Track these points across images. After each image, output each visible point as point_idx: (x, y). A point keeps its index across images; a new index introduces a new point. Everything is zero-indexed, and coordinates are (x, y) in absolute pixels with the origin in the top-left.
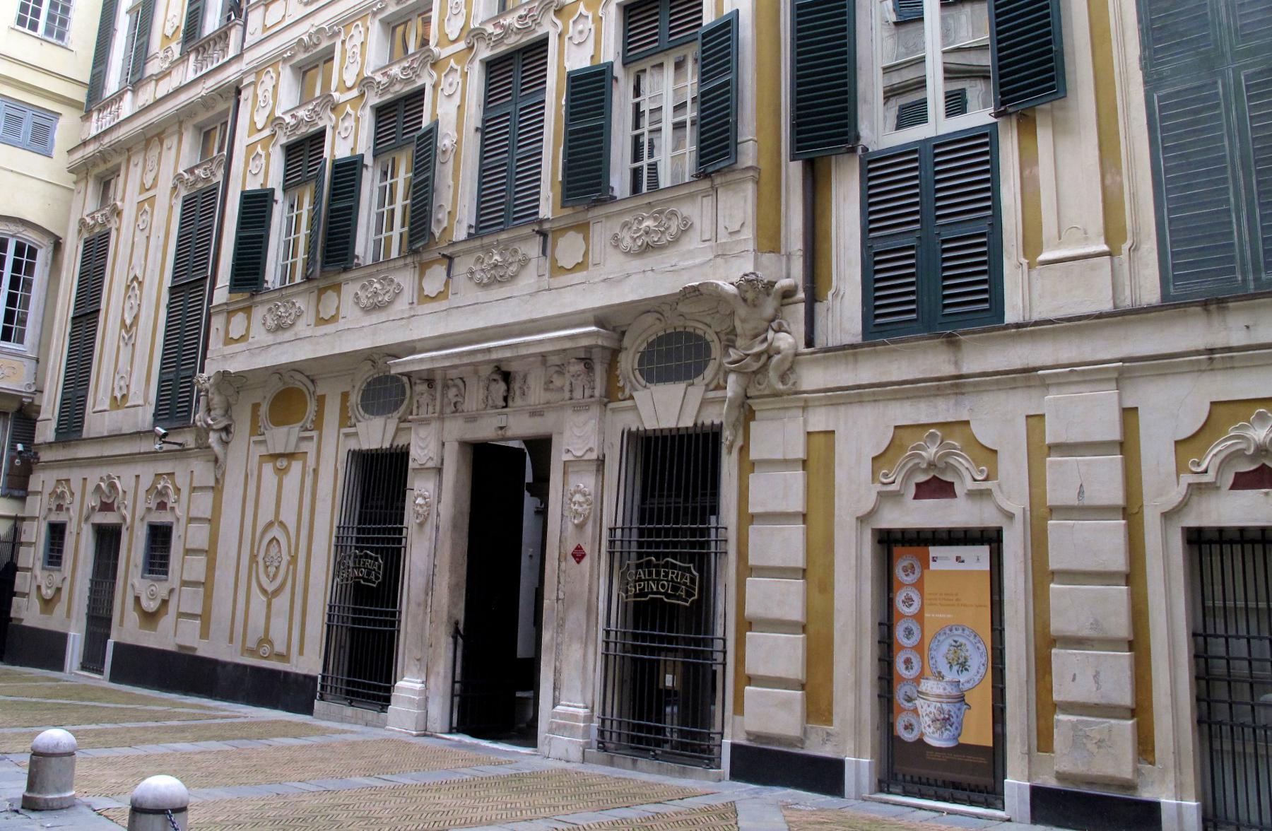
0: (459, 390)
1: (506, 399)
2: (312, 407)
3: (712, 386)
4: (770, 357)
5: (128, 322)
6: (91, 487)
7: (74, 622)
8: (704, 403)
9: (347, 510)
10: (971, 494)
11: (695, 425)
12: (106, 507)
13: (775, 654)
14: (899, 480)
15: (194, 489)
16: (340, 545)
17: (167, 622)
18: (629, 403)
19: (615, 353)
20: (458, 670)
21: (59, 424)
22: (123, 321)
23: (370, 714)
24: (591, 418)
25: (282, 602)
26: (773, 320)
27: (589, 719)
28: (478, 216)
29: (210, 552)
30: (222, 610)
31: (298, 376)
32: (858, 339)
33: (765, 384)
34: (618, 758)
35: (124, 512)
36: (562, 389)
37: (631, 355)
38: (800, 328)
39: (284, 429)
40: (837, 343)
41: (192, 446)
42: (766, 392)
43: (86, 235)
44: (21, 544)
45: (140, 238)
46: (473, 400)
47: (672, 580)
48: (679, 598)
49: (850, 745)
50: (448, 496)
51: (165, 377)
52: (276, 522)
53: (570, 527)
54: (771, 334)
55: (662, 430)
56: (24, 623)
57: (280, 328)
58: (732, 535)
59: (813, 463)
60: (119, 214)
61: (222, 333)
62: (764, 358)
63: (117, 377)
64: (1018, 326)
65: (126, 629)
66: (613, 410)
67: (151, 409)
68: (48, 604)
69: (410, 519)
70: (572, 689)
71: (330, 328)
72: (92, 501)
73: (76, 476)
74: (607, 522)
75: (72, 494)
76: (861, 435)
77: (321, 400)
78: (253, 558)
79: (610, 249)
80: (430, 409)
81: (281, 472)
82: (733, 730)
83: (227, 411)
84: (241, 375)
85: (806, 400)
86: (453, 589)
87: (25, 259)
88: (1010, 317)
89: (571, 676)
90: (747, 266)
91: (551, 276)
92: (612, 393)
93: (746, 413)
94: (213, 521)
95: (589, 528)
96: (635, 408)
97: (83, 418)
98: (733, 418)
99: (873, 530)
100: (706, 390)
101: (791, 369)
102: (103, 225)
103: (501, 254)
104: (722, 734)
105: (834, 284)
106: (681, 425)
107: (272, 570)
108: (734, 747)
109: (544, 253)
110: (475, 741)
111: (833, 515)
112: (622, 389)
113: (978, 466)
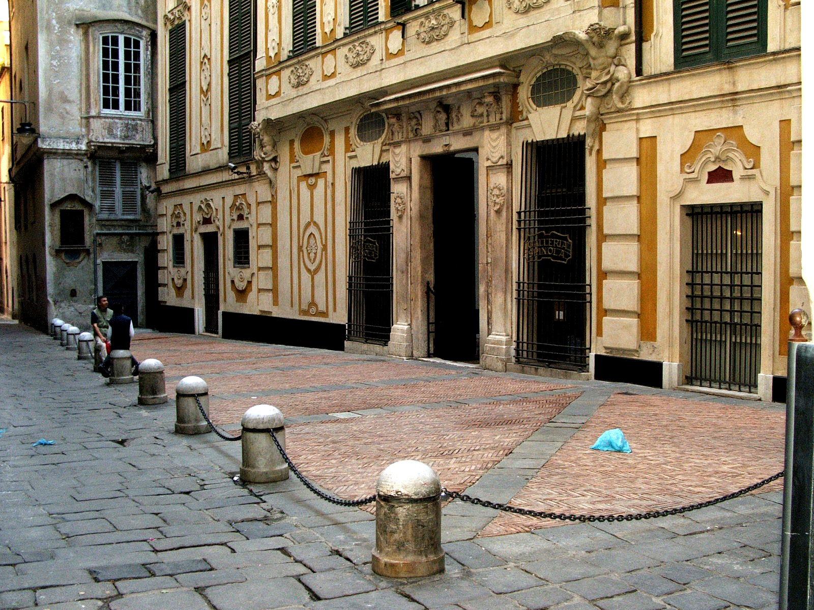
0: (418, 120)
1: (447, 125)
2: (327, 139)
3: (578, 108)
4: (613, 84)
5: (205, 88)
6: (195, 208)
7: (197, 300)
8: (574, 119)
9: (355, 211)
10: (743, 178)
11: (568, 136)
12: (207, 221)
13: (619, 294)
14: (697, 171)
15: (259, 204)
16: (352, 235)
17: (252, 296)
18: (525, 123)
19: (515, 86)
20: (432, 314)
21: (170, 166)
22: (201, 88)
23: (378, 348)
24: (501, 135)
25: (320, 277)
26: (615, 57)
27: (508, 343)
28: (351, 20)
29: (274, 247)
30: (284, 285)
31: (315, 118)
32: (672, 68)
33: (611, 103)
34: (527, 368)
35: (218, 223)
36: (482, 115)
37: (526, 88)
38: (632, 62)
39: (311, 156)
40: (658, 72)
41: (255, 174)
42: (612, 110)
43: (170, 27)
44: (159, 251)
45: (205, 25)
46: (427, 128)
47: (556, 247)
48: (561, 258)
49: (666, 354)
50: (416, 194)
51: (233, 126)
52: (312, 222)
53: (492, 214)
54: (612, 68)
55: (547, 141)
56: (167, 304)
57: (299, 85)
58: (593, 213)
59: (643, 159)
60: (189, 9)
61: (264, 92)
62: (609, 85)
63: (203, 129)
64: (774, 54)
65: (228, 304)
66: (517, 128)
67: (226, 150)
68: (180, 290)
69: (394, 215)
70: (500, 324)
71: (332, 82)
72: (198, 217)
73: (185, 201)
74: (516, 208)
75: (185, 214)
76: (673, 138)
77: (332, 134)
78: (300, 249)
79: (506, 10)
80: (400, 135)
81: (312, 187)
82: (597, 347)
83: (274, 145)
84: (279, 121)
85: (638, 114)
86: (424, 261)
87: (132, 49)
88: (772, 47)
89: (497, 316)
90: (592, 17)
91: (469, 34)
92: (515, 118)
93: (599, 124)
94: (273, 225)
95: (504, 213)
96: (529, 126)
97: (185, 160)
98: (591, 131)
99: (683, 206)
100: (574, 111)
101: (627, 91)
102: (180, 18)
103: (436, 19)
104: (590, 349)
105: (655, 28)
106: (559, 136)
107: (312, 255)
108: (597, 356)
109: (463, 16)
110: (443, 361)
111: (656, 196)
112: (521, 112)
113: (748, 158)
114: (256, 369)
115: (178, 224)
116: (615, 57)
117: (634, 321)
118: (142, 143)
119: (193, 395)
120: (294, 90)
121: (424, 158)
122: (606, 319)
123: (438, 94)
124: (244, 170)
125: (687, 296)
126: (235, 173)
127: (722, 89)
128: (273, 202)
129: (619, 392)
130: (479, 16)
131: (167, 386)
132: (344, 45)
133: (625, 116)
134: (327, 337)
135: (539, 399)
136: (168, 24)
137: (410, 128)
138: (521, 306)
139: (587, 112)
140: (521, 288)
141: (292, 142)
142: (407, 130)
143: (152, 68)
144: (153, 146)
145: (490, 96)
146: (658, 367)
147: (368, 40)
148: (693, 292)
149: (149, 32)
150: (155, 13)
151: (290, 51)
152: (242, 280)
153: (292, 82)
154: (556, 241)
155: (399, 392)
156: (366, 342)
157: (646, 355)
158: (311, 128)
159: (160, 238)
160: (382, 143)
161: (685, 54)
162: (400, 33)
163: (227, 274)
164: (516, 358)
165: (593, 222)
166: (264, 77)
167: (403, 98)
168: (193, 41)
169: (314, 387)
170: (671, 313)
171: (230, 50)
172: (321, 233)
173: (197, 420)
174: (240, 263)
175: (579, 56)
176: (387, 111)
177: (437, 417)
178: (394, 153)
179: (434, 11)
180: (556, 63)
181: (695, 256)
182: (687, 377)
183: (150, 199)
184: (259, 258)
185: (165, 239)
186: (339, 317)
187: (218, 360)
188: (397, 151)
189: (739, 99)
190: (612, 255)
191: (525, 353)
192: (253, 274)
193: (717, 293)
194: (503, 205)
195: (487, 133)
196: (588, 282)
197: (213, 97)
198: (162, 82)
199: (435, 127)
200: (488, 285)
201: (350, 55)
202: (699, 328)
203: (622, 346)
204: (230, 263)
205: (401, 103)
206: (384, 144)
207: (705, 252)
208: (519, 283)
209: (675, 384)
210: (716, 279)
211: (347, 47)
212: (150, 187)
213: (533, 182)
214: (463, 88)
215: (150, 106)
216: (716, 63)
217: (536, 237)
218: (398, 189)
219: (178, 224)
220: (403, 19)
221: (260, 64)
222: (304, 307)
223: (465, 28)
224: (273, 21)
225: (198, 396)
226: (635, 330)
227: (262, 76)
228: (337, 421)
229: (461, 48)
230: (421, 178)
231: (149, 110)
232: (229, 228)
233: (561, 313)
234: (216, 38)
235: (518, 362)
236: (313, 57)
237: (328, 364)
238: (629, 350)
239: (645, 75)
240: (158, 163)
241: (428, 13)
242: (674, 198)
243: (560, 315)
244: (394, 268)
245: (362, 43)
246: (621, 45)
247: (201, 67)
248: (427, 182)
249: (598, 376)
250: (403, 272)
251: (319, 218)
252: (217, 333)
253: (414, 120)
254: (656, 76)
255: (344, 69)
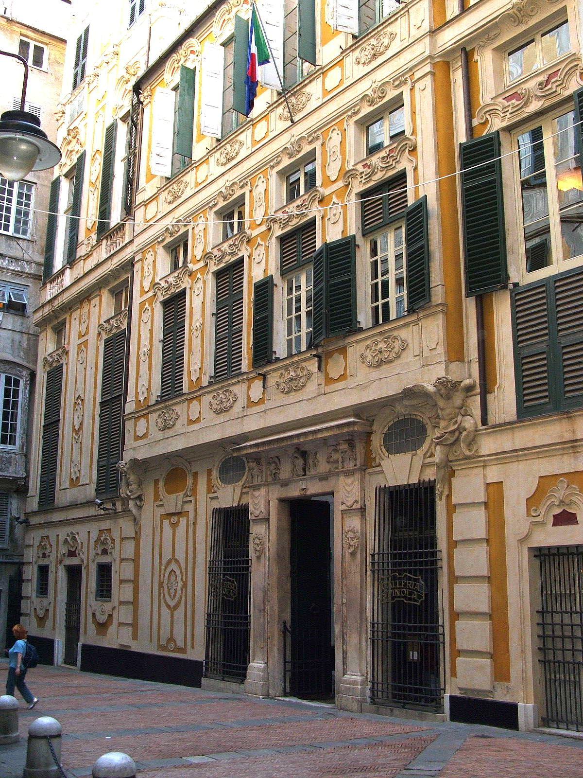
1: (304, 470)
2: (190, 481)
5: (77, 427)
6: (61, 541)
7: (57, 630)
8: (424, 466)
9: (215, 550)
11: (419, 481)
12: (72, 554)
13: (472, 634)
14: (542, 514)
15: (123, 539)
17: (112, 629)
18: (378, 469)
19: (369, 434)
20: (288, 653)
21: (40, 499)
22: (74, 427)
23: (234, 686)
25: (179, 614)
27: (363, 683)
29: (135, 582)
32: (515, 418)
33: (459, 451)
34: (382, 709)
35: (82, 556)
36: (337, 461)
38: (477, 412)
39: (174, 495)
40: (502, 421)
42: (461, 458)
46: (285, 472)
47: (409, 589)
51: (101, 464)
52: (173, 559)
53: (347, 555)
54: (459, 418)
57: (165, 428)
58: (444, 555)
59: (491, 505)
60: (67, 353)
61: (132, 434)
62: (457, 434)
63: (73, 465)
65: (89, 636)
67: (94, 486)
68: (41, 621)
69: (252, 555)
70: (355, 666)
71: (196, 427)
72: (64, 550)
73: (52, 533)
74: (370, 551)
76: (519, 482)
77: (195, 476)
78: (161, 585)
79: (359, 364)
81: (174, 526)
82: (451, 689)
83: (140, 484)
84: (145, 461)
85: (485, 461)
86: (281, 601)
89: (352, 655)
90: (439, 371)
92: (369, 464)
93: (449, 471)
94: (136, 560)
95: (358, 556)
96: (382, 472)
101: (473, 440)
102: (58, 361)
103: (295, 371)
104: (444, 690)
105: (498, 381)
107: (172, 591)
108: (451, 697)
109: (320, 369)
110: (299, 701)
114: (111, 706)
115: (44, 555)
116: (462, 408)
117: (487, 662)
118: (15, 475)
119: (45, 737)
120: (161, 432)
121: (282, 501)
122: (459, 660)
123: (295, 441)
124: (109, 506)
125: (539, 636)
126: (101, 509)
127: (563, 438)
128: (137, 539)
129: (475, 734)
130: (335, 368)
131: (20, 723)
132: (208, 393)
133: (473, 463)
134: (183, 673)
135: (394, 742)
136: (47, 366)
137: (269, 472)
138: (376, 659)
139: (436, 459)
140: (376, 637)
141: (156, 482)
142: (266, 473)
143: (29, 406)
144: (25, 478)
145: (345, 444)
146: (512, 709)
147: (231, 389)
148: (544, 632)
149: (29, 372)
150: (36, 355)
151: (158, 396)
152: (103, 613)
153: (158, 424)
154: (409, 583)
155: (253, 734)
156: (223, 680)
157: (501, 696)
158: (175, 469)
159: (25, 568)
160: (243, 486)
161: (526, 404)
162: (261, 383)
163: (88, 607)
164: (371, 698)
165: (444, 564)
166: (133, 420)
167: (263, 444)
168: (69, 382)
169: (169, 727)
170: (523, 652)
171: (103, 392)
172: (181, 572)
173: (48, 765)
174: (102, 596)
175: (428, 406)
176: (248, 456)
177: (292, 763)
178: (254, 496)
179: (293, 363)
180: (407, 412)
181: (545, 597)
182: (543, 719)
183: (19, 529)
184: (121, 592)
185: (31, 569)
186: (197, 653)
187: (75, 694)
188: (257, 493)
189: (579, 446)
190: (463, 597)
191: (380, 693)
192: (115, 607)
193: (568, 633)
194: (358, 547)
195: (342, 478)
196: (440, 623)
197: (85, 435)
198: (37, 418)
199: (293, 471)
200: (343, 626)
201: (214, 402)
202: (552, 668)
203: (477, 687)
204: (92, 597)
205: (261, 449)
206: (244, 487)
207: (554, 592)
208: (373, 624)
209: (532, 726)
210: (567, 619)
211: (212, 395)
212: (19, 518)
213: (386, 527)
214: (320, 436)
215: (24, 440)
216: (556, 413)
217: (390, 579)
218: (257, 530)
219: (44, 555)
220: (265, 370)
221: (130, 407)
222: (163, 642)
223: (322, 380)
224: (144, 367)
225: (50, 737)
226: (488, 670)
227: (130, 418)
228: (191, 765)
229: (318, 398)
230: (279, 520)
231: (23, 445)
232: (93, 561)
233: (415, 653)
234: (90, 381)
235: (373, 702)
236: (180, 402)
237: (184, 702)
238: (485, 691)
239: (490, 424)
240: (29, 495)
241: (288, 365)
242: (522, 541)
243: (414, 655)
244: (252, 609)
245: (226, 391)
246: (467, 397)
247: (75, 407)
248: (286, 524)
249: (453, 718)
250: (260, 611)
251: (180, 556)
252: (75, 665)
253: (274, 465)
254: (500, 425)
255: (208, 416)
